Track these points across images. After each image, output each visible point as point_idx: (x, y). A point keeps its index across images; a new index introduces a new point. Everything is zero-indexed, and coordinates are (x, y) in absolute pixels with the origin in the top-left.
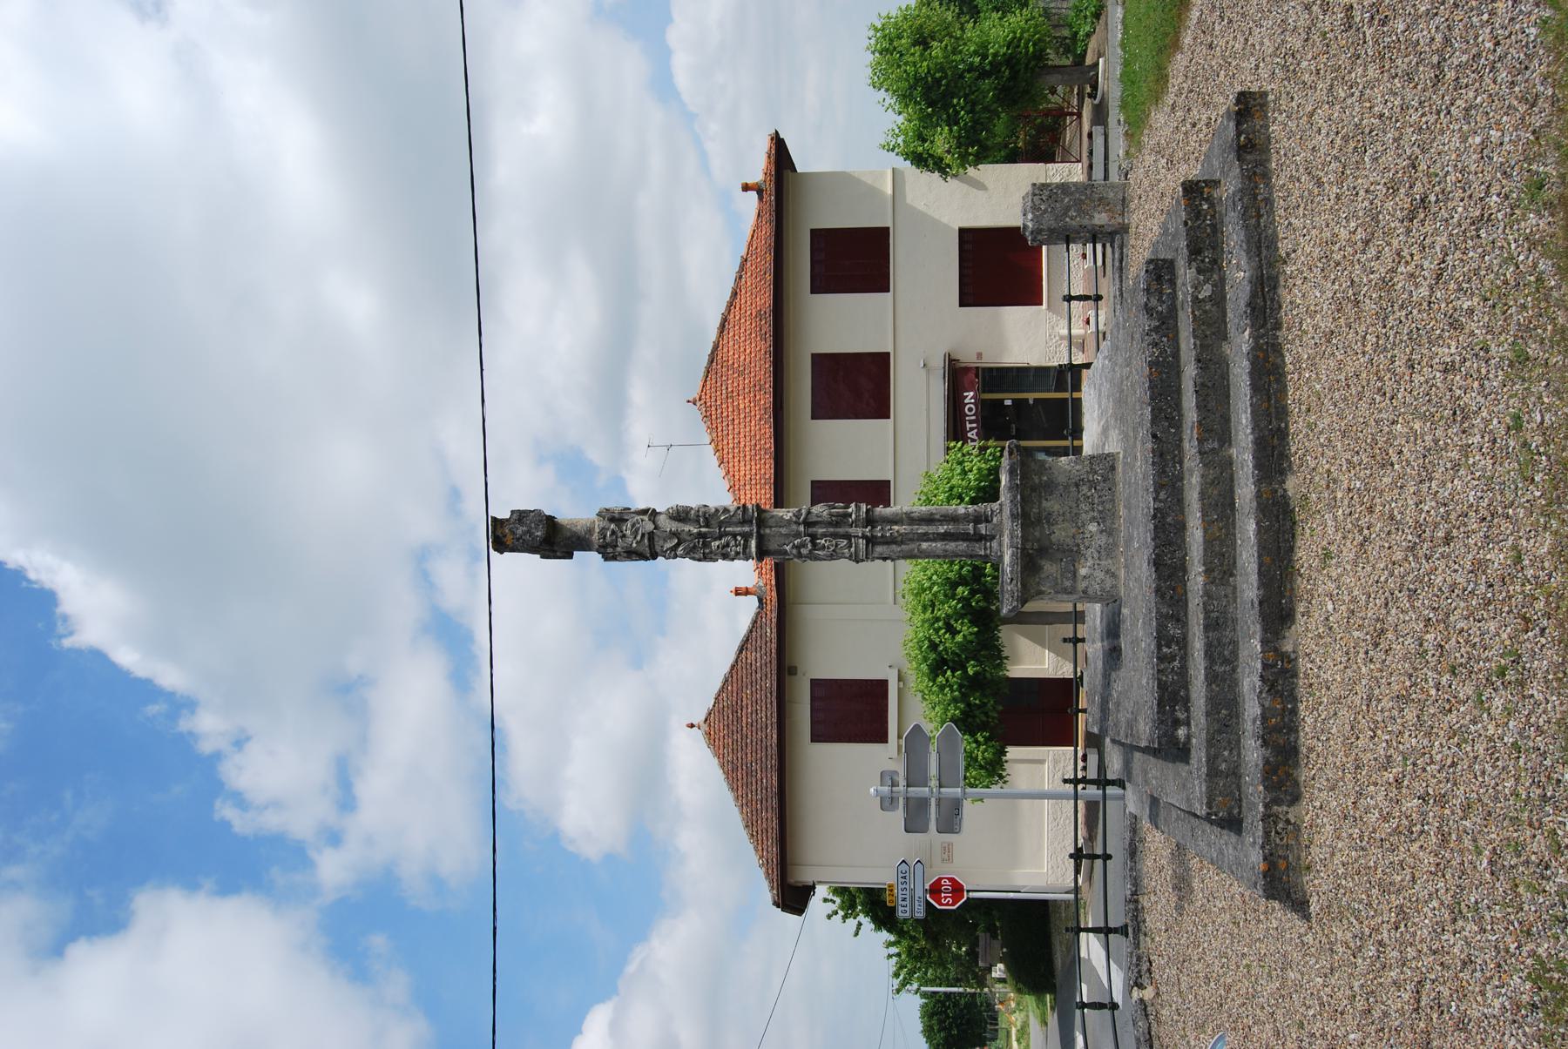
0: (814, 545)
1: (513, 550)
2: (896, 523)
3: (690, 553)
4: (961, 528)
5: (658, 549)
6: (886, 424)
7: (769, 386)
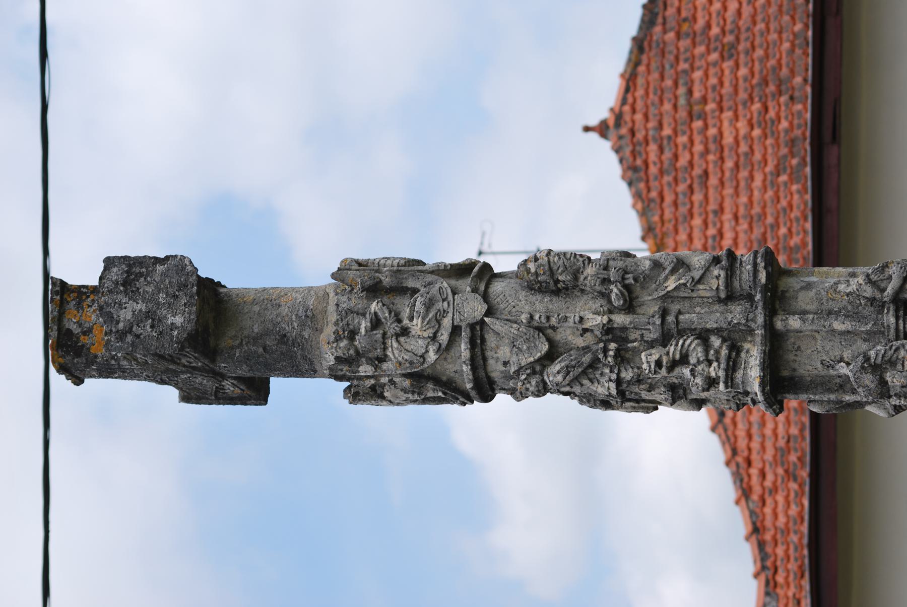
1: (107, 371)
3: (577, 385)
5: (495, 369)
7: (801, 83)
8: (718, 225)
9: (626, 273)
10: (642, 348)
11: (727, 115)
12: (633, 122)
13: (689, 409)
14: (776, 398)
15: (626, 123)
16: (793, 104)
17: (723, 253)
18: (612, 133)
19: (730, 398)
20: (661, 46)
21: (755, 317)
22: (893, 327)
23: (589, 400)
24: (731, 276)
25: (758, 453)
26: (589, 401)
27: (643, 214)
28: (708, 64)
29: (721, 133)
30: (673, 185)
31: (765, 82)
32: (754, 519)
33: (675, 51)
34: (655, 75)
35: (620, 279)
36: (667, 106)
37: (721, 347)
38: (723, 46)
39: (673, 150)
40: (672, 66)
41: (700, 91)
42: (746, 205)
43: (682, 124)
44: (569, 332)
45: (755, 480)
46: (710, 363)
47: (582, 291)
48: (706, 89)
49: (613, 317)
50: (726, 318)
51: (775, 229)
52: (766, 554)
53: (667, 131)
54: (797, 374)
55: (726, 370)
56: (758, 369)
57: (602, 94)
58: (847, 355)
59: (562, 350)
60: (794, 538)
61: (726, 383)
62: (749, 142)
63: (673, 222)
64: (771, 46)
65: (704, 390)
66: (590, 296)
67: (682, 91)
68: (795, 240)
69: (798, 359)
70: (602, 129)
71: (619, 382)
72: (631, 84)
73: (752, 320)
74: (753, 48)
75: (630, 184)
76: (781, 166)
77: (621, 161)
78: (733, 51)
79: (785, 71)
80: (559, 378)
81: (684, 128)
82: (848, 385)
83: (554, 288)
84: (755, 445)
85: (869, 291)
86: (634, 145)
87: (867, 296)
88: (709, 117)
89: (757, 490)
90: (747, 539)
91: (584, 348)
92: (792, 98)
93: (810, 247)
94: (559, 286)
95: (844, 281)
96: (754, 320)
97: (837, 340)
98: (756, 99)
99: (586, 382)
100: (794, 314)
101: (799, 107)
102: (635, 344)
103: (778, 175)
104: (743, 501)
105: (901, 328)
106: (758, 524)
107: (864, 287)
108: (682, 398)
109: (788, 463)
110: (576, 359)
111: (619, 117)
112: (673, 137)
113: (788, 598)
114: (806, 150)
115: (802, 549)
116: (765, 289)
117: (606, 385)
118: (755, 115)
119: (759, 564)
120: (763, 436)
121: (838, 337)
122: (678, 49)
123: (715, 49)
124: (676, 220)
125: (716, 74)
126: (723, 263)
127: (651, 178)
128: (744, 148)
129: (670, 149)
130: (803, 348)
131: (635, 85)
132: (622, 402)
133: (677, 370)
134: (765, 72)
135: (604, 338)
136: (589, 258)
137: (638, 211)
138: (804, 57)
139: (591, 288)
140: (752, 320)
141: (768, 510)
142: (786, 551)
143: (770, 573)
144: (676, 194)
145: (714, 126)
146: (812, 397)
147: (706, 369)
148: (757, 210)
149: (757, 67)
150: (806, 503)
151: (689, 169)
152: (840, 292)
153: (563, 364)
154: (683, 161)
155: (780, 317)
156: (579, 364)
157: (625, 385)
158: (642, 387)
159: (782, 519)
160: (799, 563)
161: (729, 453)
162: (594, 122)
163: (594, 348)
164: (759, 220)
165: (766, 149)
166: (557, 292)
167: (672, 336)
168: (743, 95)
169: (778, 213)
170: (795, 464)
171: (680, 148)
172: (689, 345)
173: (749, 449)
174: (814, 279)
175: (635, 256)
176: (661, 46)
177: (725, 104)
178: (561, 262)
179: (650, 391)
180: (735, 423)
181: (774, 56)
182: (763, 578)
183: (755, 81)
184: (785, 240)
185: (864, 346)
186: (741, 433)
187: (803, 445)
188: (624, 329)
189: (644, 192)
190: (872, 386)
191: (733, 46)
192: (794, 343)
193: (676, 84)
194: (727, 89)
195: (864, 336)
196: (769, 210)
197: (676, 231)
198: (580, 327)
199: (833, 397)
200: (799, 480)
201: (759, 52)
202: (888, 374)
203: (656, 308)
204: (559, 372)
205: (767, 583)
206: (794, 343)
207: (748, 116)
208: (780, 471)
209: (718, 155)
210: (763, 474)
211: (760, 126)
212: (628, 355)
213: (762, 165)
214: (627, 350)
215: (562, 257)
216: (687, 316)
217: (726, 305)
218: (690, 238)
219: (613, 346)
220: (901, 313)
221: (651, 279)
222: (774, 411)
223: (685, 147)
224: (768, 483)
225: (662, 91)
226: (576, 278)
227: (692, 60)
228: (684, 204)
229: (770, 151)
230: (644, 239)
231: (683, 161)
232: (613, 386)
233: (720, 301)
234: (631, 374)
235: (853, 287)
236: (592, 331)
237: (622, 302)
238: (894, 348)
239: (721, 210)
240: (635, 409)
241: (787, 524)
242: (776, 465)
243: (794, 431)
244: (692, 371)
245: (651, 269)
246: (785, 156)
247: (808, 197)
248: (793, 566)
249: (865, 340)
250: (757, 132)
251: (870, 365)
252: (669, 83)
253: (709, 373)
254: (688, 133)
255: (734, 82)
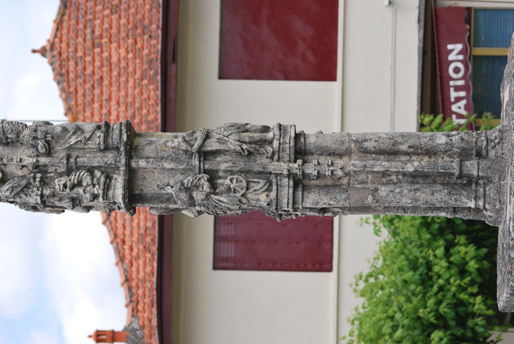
0: (213, 186)
2: (341, 156)
4: (443, 162)
6: (332, 88)
7: (156, 28)
8: (108, 108)
9: (47, 134)
10: (55, 177)
11: (114, 45)
12: (61, 48)
13: (82, 212)
14: (131, 206)
15: (56, 48)
16: (151, 40)
17: (102, 123)
18: (48, 54)
19: (106, 206)
20: (77, 5)
21: (120, 160)
22: (197, 166)
23: (25, 206)
24: (107, 137)
25: (129, 237)
26: (25, 207)
27: (66, 100)
28: (103, 16)
29: (110, 56)
30: (83, 84)
31: (136, 27)
32: (126, 274)
33: (85, 8)
34: (73, 22)
35: (44, 137)
36: (80, 40)
37: (100, 177)
38: (112, 6)
39: (83, 64)
40: (83, 17)
41: (99, 31)
42: (124, 97)
43: (88, 50)
44: (13, 167)
45: (127, 252)
46: (94, 186)
47: (22, 144)
48: (102, 30)
49: (39, 159)
50: (104, 160)
51: (140, 110)
52: (132, 293)
53: (80, 54)
54: (144, 192)
55: (104, 190)
56: (121, 189)
57: (43, 32)
58: (172, 182)
59: (9, 177)
60: (148, 285)
61: (103, 197)
62: (126, 61)
63: (83, 105)
64: (139, 7)
65: (90, 201)
66: (26, 146)
67: (88, 31)
68: (151, 117)
69: (144, 184)
70: (43, 52)
71: (42, 196)
72: (59, 26)
73: (118, 162)
74: (129, 8)
75: (59, 83)
76: (144, 75)
77: (54, 70)
78: (118, 9)
79: (146, 22)
80: (8, 193)
81: (90, 52)
82: (172, 199)
83: (5, 142)
84: (127, 232)
85: (184, 146)
86: (61, 61)
87: (183, 149)
88: (104, 46)
89: (128, 257)
90: (122, 285)
91: (22, 177)
92: (150, 37)
93: (159, 121)
94: (8, 140)
95: (173, 140)
96: (119, 162)
97: (166, 173)
98: (131, 37)
99: (23, 196)
100: (142, 158)
101: (154, 42)
102: (52, 174)
103: (142, 80)
104: (120, 264)
105: (202, 167)
106: (129, 277)
107: (182, 144)
108: (78, 205)
109: (146, 242)
110: (17, 182)
111: (52, 45)
112: (83, 57)
113: (144, 318)
114: (158, 66)
115: (153, 291)
116: (126, 144)
117: (35, 197)
118: (130, 46)
119: (128, 299)
120: (132, 227)
121: (167, 172)
122: (86, 7)
123: (108, 8)
124: (85, 104)
125: (108, 22)
126: (103, 129)
127: (71, 80)
128: (123, 64)
129: (82, 64)
130: (147, 178)
131: (62, 27)
132: (44, 208)
133: (76, 190)
134: (135, 21)
135: (34, 171)
136: (26, 125)
137: (63, 99)
138: (157, 14)
139: (27, 142)
140: (118, 162)
141: (134, 269)
142: (144, 292)
143: (134, 304)
144: (85, 89)
145: (107, 51)
146: (152, 205)
147: (92, 189)
148: (130, 99)
149: (131, 18)
150: (155, 265)
151: (92, 76)
152: (168, 146)
153: (10, 185)
154: (89, 71)
155: (134, 160)
156: (19, 185)
157: (45, 198)
158: (55, 199)
159: (142, 274)
160: (151, 298)
161: (113, 236)
162: (38, 47)
163: (28, 176)
164: (131, 105)
165: (135, 65)
166: (7, 144)
167: (73, 170)
168: (123, 34)
169: (142, 101)
170: (149, 243)
171: (87, 63)
172: (83, 176)
173: (124, 235)
174: (154, 139)
175: (52, 124)
176: (77, 5)
177: (113, 39)
178: (9, 127)
179: (60, 201)
180: (116, 220)
181: (141, 12)
182: (130, 307)
183: (130, 27)
184: (146, 116)
185: (181, 177)
186: (119, 225)
187: (154, 232)
188: (45, 166)
189: (66, 88)
190: (185, 199)
191: (118, 6)
192: (142, 175)
193: (85, 27)
194: (114, 31)
195: (181, 171)
196: (137, 100)
197: (84, 111)
198: (20, 164)
199: (163, 205)
200: (152, 252)
201: (132, 10)
202: (194, 193)
203: (64, 154)
204: (7, 190)
205: (133, 310)
206: (142, 175)
207: (126, 46)
208: (141, 247)
209: (109, 68)
210: (131, 249)
211: (132, 52)
212: (47, 181)
213: (133, 74)
214: (47, 178)
215: (10, 124)
216: (82, 159)
217: (104, 153)
218: (92, 114)
219: (39, 175)
220: (202, 159)
221: (61, 137)
222: (131, 213)
223: (90, 63)
224: (134, 254)
225: (77, 30)
226: (18, 136)
227: (94, 13)
228: (89, 95)
229: (138, 66)
230: (66, 114)
231: (89, 71)
232: (38, 198)
233: (100, 150)
234: (49, 192)
235: (176, 144)
236: (27, 167)
237: (44, 150)
238: (198, 178)
239: (110, 99)
240: (51, 212)
241: (144, 277)
242: (139, 243)
243: (149, 224)
244: (84, 190)
245: (62, 132)
246: (146, 69)
247: (159, 93)
248: (147, 300)
249: (182, 174)
250: (130, 55)
251: (185, 188)
252: (81, 26)
253: (94, 191)
254: (92, 55)
255: (118, 27)
